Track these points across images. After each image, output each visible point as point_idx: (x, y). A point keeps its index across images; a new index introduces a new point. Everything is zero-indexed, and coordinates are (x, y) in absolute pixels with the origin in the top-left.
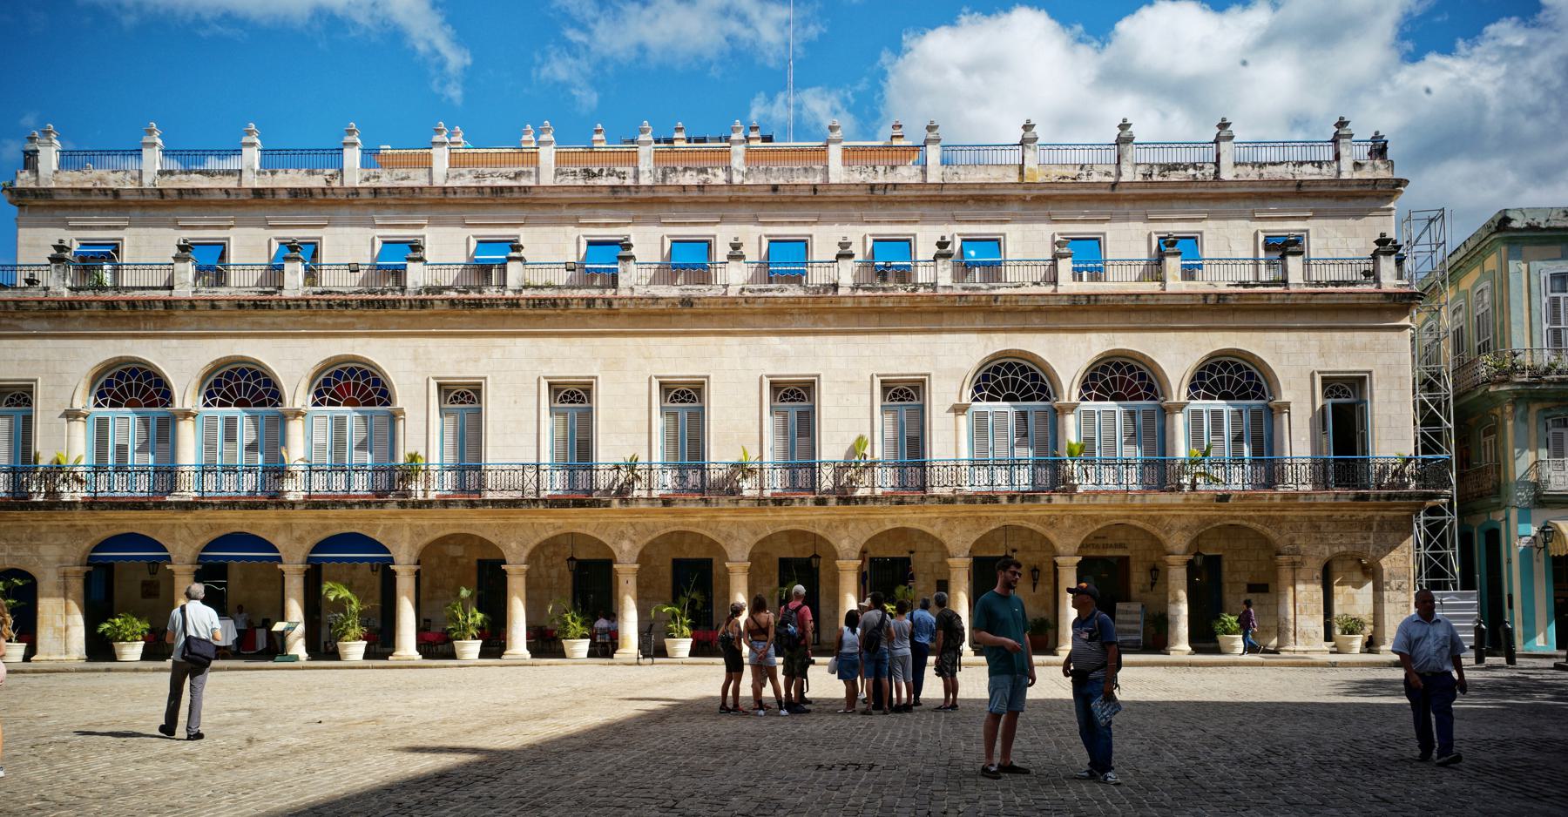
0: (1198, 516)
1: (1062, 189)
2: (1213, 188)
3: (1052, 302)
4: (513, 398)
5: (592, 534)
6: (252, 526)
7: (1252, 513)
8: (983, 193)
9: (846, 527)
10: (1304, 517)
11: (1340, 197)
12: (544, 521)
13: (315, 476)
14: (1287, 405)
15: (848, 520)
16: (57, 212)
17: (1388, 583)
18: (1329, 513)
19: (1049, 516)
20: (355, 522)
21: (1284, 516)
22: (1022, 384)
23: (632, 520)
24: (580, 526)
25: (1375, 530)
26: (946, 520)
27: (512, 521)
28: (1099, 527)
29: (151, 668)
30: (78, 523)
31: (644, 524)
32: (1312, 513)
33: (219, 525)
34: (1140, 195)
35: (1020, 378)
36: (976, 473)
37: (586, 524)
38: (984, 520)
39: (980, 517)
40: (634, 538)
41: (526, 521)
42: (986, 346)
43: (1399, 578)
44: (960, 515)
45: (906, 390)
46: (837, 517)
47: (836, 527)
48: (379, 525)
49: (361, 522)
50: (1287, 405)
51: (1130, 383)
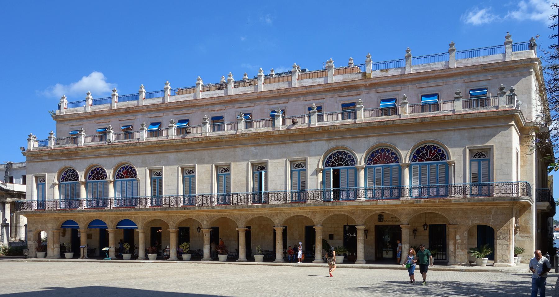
0: (413, 209)
1: (380, 80)
2: (444, 72)
3: (453, 118)
4: (171, 173)
5: (194, 219)
6: (99, 217)
7: (436, 208)
8: (349, 85)
9: (277, 215)
10: (460, 208)
11: (505, 70)
12: (180, 215)
13: (435, 190)
14: (453, 162)
15: (278, 212)
16: (66, 122)
17: (499, 237)
18: (472, 207)
19: (352, 210)
20: (126, 216)
21: (451, 209)
22: (423, 154)
23: (206, 214)
24: (191, 216)
25: (493, 214)
26: (313, 212)
27: (170, 215)
28: (372, 214)
29: (257, 264)
30: (56, 217)
31: (210, 215)
32: (463, 207)
33: (91, 217)
34: (413, 78)
35: (132, 172)
36: (415, 191)
37: (193, 215)
38: (327, 212)
39: (325, 211)
40: (207, 220)
41: (174, 215)
42: (328, 145)
43: (504, 234)
44: (318, 210)
45: (301, 164)
46: (274, 212)
47: (274, 215)
48: (133, 216)
49: (128, 216)
50: (453, 162)
51: (434, 153)
